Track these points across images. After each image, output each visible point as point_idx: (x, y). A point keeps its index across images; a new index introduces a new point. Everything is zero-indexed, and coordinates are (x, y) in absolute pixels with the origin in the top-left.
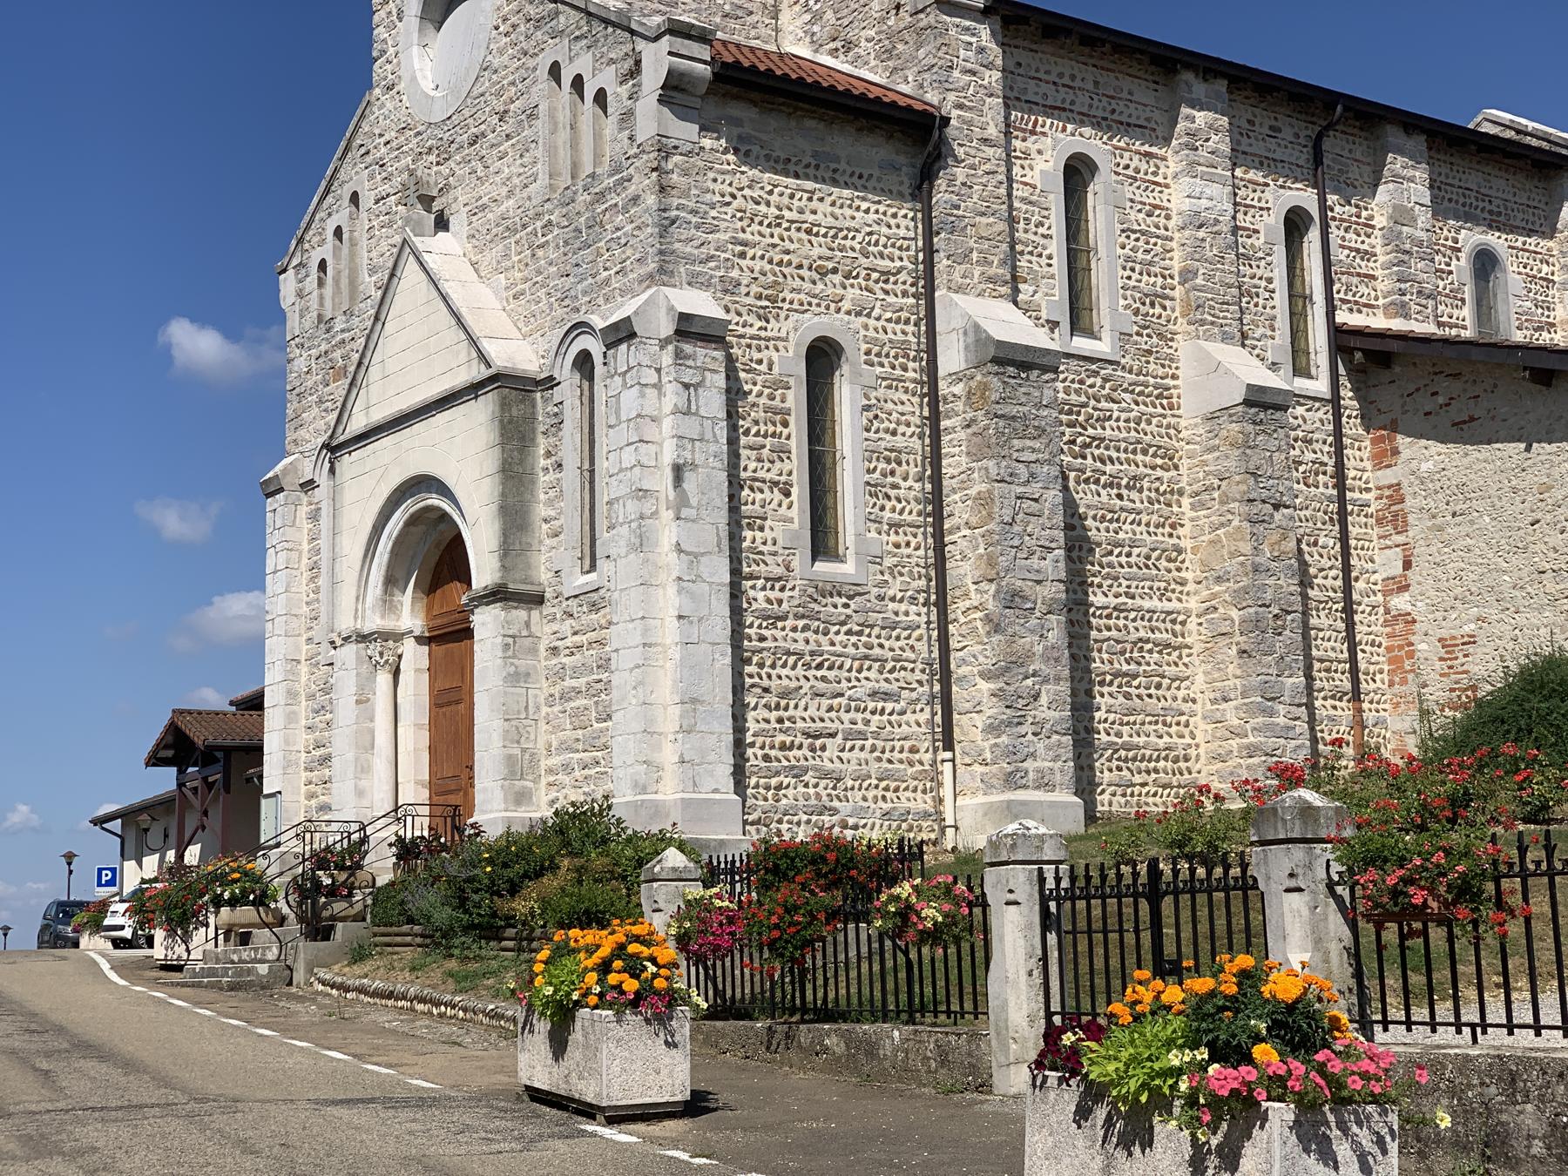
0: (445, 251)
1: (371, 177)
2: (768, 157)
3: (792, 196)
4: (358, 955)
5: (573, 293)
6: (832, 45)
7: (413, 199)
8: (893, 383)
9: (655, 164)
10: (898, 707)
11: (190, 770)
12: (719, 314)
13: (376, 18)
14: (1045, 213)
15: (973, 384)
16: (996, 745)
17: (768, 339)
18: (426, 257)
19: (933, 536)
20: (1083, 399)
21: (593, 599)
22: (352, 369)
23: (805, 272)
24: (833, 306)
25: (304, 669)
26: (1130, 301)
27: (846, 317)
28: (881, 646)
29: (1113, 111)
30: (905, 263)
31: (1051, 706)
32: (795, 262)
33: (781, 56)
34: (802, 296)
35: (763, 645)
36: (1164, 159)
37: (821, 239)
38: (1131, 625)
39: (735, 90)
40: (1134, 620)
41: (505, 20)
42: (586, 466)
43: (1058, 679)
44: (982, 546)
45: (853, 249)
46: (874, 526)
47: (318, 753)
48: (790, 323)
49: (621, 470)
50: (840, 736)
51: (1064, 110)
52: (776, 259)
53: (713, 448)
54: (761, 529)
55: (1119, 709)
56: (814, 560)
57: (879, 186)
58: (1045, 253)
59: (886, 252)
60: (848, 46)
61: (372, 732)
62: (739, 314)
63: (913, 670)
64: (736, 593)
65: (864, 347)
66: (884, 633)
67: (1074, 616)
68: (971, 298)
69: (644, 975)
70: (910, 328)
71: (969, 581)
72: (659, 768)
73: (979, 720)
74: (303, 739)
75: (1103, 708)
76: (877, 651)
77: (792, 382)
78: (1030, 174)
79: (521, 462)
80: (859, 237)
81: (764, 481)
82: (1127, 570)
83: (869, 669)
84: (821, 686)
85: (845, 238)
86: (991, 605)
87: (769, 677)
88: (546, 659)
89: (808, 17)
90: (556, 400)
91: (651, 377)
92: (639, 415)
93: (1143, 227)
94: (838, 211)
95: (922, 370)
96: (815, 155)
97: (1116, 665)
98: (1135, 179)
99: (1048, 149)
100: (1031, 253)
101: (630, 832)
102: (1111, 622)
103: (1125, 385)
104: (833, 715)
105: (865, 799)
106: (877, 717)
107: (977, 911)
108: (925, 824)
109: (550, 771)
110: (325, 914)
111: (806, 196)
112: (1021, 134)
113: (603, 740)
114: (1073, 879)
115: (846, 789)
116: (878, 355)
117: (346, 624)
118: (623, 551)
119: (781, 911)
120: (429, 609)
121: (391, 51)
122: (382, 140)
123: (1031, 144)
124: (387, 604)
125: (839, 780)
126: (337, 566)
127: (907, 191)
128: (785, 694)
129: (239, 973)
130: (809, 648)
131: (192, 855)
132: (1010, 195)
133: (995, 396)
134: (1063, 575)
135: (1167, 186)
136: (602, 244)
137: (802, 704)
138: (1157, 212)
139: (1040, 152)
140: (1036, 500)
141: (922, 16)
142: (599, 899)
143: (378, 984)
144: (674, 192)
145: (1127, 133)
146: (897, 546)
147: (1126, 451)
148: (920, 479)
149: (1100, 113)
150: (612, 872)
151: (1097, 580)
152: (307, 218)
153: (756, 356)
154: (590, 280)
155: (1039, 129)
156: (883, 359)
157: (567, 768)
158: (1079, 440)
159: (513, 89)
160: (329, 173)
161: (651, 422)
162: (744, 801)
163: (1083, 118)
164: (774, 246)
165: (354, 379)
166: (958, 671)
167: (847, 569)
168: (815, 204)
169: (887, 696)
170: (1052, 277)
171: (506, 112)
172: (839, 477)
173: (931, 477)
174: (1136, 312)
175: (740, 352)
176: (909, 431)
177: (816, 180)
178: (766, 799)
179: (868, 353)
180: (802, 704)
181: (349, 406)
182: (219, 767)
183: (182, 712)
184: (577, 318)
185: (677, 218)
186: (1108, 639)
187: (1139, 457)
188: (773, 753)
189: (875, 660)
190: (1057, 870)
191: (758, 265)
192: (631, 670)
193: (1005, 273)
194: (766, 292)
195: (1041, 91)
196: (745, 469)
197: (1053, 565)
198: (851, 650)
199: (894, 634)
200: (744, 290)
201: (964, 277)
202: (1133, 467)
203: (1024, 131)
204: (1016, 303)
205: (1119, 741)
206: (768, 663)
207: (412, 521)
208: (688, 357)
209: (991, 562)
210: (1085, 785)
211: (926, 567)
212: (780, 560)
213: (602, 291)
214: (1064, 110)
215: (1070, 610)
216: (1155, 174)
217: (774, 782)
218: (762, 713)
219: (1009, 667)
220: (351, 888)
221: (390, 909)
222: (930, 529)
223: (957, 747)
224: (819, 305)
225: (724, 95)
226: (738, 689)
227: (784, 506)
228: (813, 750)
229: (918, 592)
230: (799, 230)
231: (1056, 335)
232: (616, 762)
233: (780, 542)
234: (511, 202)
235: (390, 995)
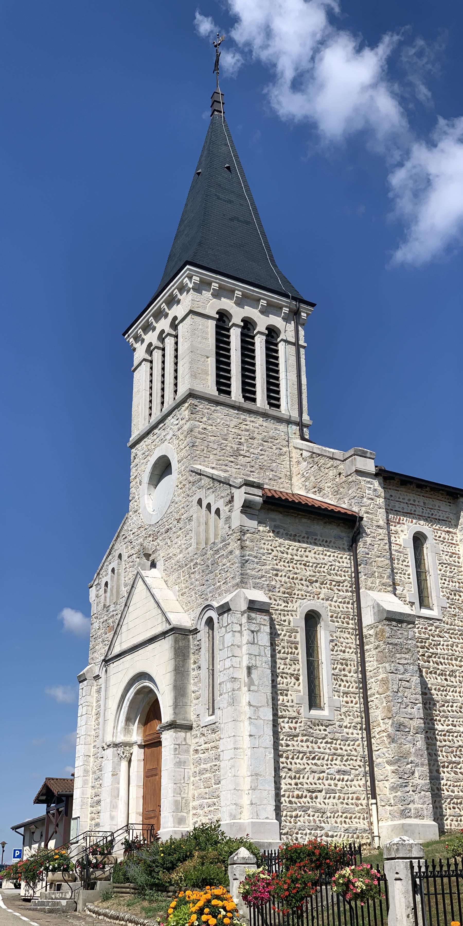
0: (154, 576)
1: (127, 547)
2: (287, 534)
3: (297, 550)
4: (106, 897)
5: (205, 592)
6: (314, 490)
7: (142, 555)
8: (343, 630)
9: (239, 537)
10: (350, 778)
11: (52, 805)
12: (267, 600)
13: (131, 485)
14: (406, 556)
15: (378, 630)
16: (396, 796)
17: (288, 611)
18: (146, 579)
19: (363, 698)
20: (427, 636)
21: (213, 728)
22: (115, 627)
23: (303, 582)
24: (316, 596)
25: (92, 759)
26: (445, 593)
27: (322, 601)
28: (341, 749)
29: (432, 514)
30: (347, 577)
31: (420, 778)
32: (299, 578)
33: (293, 495)
34: (303, 592)
35: (288, 748)
36: (455, 534)
37: (310, 568)
38: (455, 739)
39: (273, 507)
40: (456, 737)
41: (181, 483)
42: (211, 668)
43: (422, 765)
44: (385, 702)
45: (324, 572)
46: (336, 694)
47: (96, 799)
48: (298, 604)
49: (225, 669)
50: (324, 791)
51: (411, 514)
52: (291, 576)
53: (264, 659)
54: (286, 695)
55: (452, 779)
56: (310, 709)
57: (334, 545)
58: (407, 573)
59: (338, 573)
60: (320, 490)
61: (118, 789)
62: (275, 600)
63: (356, 760)
64: (275, 724)
65: (330, 614)
66: (342, 743)
67: (429, 735)
68: (376, 592)
69: (219, 916)
70: (350, 606)
71: (380, 718)
72: (241, 807)
73: (387, 784)
74: (90, 792)
75: (445, 779)
76: (339, 751)
77: (299, 630)
78: (398, 540)
79: (183, 666)
80: (327, 567)
81: (287, 674)
82: (451, 713)
83: (336, 760)
84: (314, 768)
85: (321, 567)
86: (390, 730)
87: (291, 763)
88: (193, 755)
89: (304, 479)
90: (198, 639)
91: (238, 628)
92: (232, 645)
93: (448, 562)
94: (317, 556)
95: (355, 624)
96: (307, 533)
97: (450, 758)
98: (444, 542)
99: (405, 530)
100: (401, 573)
101: (228, 838)
102: (446, 738)
103: (445, 630)
104: (320, 781)
105: (336, 822)
106: (340, 782)
107: (382, 882)
108: (365, 835)
109: (194, 808)
110: (92, 877)
111: (303, 550)
112: (394, 524)
113: (217, 793)
114: (427, 867)
115: (327, 818)
116: (336, 617)
117: (109, 739)
118: (226, 705)
119: (289, 881)
120: (145, 731)
121: (137, 497)
122: (132, 532)
123: (398, 528)
124: (127, 730)
125: (324, 813)
126: (106, 713)
127: (346, 547)
128: (298, 772)
129: (54, 904)
130: (309, 750)
131: (52, 844)
132: (390, 549)
133: (387, 635)
134: (422, 716)
135: (458, 545)
136: (217, 571)
137: (306, 776)
138: (454, 556)
139: (402, 531)
140: (408, 681)
141: (350, 477)
142: (212, 872)
143: (113, 912)
144: (247, 549)
145: (439, 523)
146: (347, 703)
147: (447, 659)
148: (356, 672)
149: (427, 515)
150: (218, 859)
151: (438, 718)
152: (101, 565)
153: (283, 618)
154: (213, 587)
155: (401, 522)
156: (339, 619)
157: (201, 807)
158: (426, 654)
159: (183, 510)
160: (111, 546)
161: (238, 647)
162: (280, 823)
163: (420, 517)
164: (290, 571)
165: (116, 631)
166: (377, 761)
167: (325, 713)
168: (307, 553)
169: (345, 772)
170: (410, 583)
171: (180, 519)
172: (320, 672)
173: (361, 671)
174: (448, 598)
175: (276, 617)
176: (351, 651)
177: (307, 543)
178: (290, 822)
179: (332, 617)
180: (306, 776)
181: (113, 643)
182: (63, 804)
183: (49, 779)
184: (207, 603)
185: (249, 560)
186: (445, 746)
187: (454, 662)
188: (293, 800)
189: (339, 756)
190: (419, 862)
191: (283, 579)
192: (229, 760)
193: (390, 581)
194: (287, 591)
195: (401, 506)
196: (279, 668)
197: (418, 711)
198: (328, 751)
199: (347, 743)
200: (277, 590)
201: (372, 583)
202: (451, 666)
203: (395, 522)
204: (395, 595)
205: (453, 794)
206: (290, 757)
207: (138, 693)
208: (253, 619)
209: (389, 711)
210: (438, 816)
211: (360, 712)
212: (295, 709)
213: (217, 591)
214: (411, 514)
215: (427, 732)
216: (452, 540)
217: (294, 814)
218: (288, 781)
219: (400, 759)
220: (104, 864)
221: (121, 875)
222: (361, 695)
223: (378, 797)
224: (310, 596)
225: (268, 510)
226: (277, 769)
227: (297, 685)
228: (311, 798)
229: (357, 724)
230: (300, 564)
231: (414, 608)
232: (222, 804)
233: (295, 701)
234: (181, 555)
235: (117, 918)
